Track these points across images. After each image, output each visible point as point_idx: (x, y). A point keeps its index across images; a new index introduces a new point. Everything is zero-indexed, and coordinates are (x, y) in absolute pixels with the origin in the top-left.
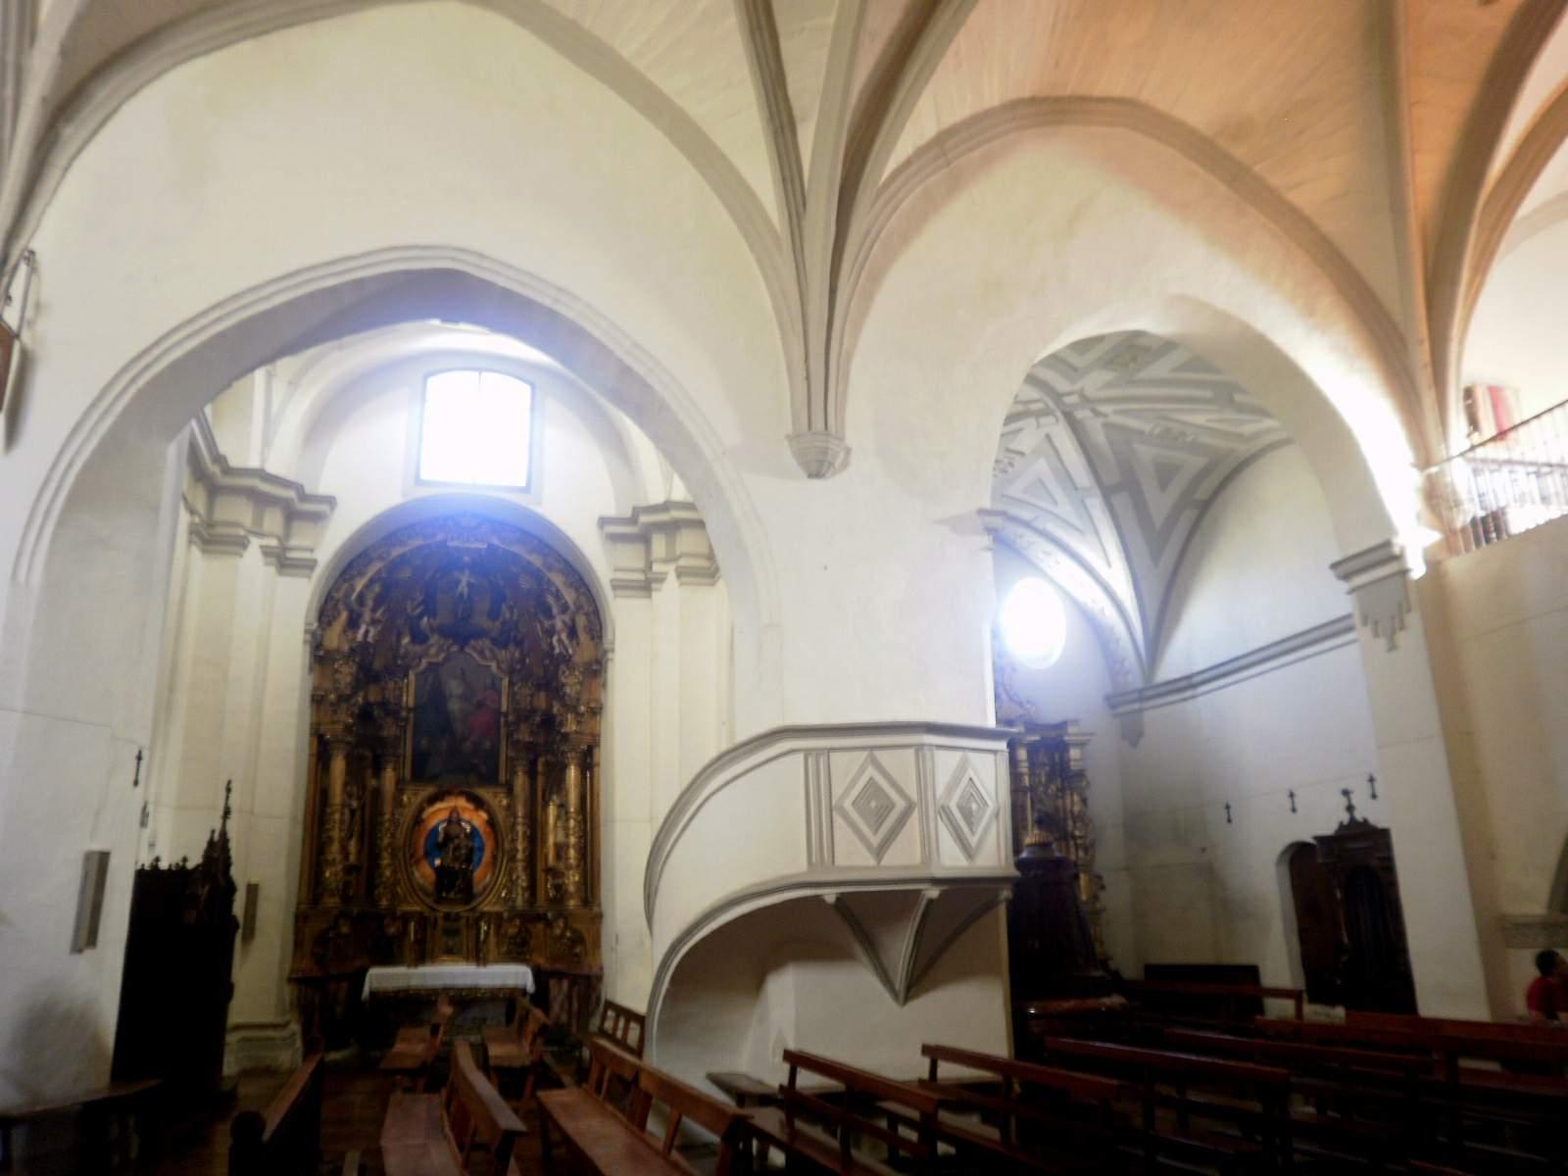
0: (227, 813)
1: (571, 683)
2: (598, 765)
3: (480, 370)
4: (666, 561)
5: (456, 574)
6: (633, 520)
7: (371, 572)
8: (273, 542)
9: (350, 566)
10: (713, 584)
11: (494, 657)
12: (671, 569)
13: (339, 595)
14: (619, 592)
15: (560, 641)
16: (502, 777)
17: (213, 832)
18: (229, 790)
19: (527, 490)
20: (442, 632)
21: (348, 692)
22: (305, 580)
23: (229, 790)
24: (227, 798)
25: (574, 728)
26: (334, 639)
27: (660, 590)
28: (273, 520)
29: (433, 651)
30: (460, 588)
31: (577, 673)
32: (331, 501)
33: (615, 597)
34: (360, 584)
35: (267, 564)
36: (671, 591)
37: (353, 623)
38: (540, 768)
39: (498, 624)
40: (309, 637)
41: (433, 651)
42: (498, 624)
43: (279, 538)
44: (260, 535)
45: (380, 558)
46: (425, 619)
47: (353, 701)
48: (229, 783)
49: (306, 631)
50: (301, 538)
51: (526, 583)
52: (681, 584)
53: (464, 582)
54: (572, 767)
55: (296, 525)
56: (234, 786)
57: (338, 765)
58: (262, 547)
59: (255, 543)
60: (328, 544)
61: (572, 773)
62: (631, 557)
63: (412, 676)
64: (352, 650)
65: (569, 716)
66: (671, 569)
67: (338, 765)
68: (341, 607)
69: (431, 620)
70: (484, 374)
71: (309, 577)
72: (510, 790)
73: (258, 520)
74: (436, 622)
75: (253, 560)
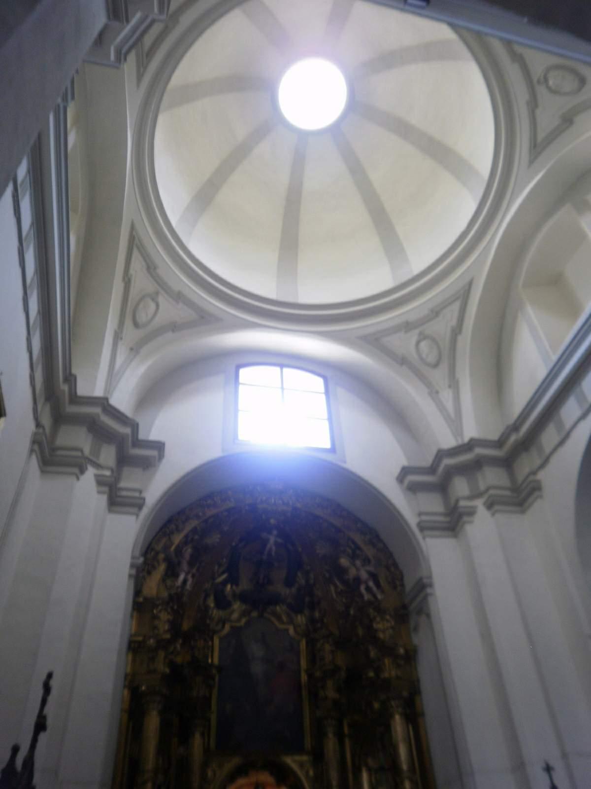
0: (41, 725)
1: (383, 627)
2: (423, 714)
3: (282, 366)
4: (471, 498)
5: (264, 535)
6: (432, 470)
7: (188, 527)
8: (107, 473)
9: (170, 521)
10: (523, 512)
11: (291, 621)
12: (479, 503)
13: (159, 547)
14: (427, 533)
15: (368, 589)
16: (308, 743)
17: (15, 749)
18: (47, 689)
19: (333, 450)
20: (243, 597)
21: (168, 636)
22: (134, 518)
23: (47, 689)
24: (44, 702)
25: (393, 673)
26: (152, 587)
27: (471, 522)
28: (108, 455)
29: (235, 616)
30: (268, 546)
31: (388, 617)
32: (159, 447)
33: (424, 538)
34: (177, 539)
35: (99, 492)
36: (483, 526)
37: (172, 572)
38: (346, 730)
39: (294, 590)
40: (134, 572)
41: (235, 616)
42: (294, 590)
43: (112, 471)
44: (98, 466)
45: (198, 517)
46: (229, 587)
47: (171, 649)
48: (50, 676)
49: (132, 566)
50: (130, 481)
51: (322, 549)
52: (493, 515)
53: (272, 539)
54: (397, 717)
55: (126, 470)
56: (53, 683)
57: (153, 722)
58: (96, 476)
59: (91, 472)
60: (156, 486)
61: (398, 725)
62: (433, 504)
63: (216, 641)
64: (171, 597)
65: (386, 661)
66: (479, 503)
67: (153, 722)
68: (161, 556)
69: (234, 587)
70: (285, 370)
71: (137, 516)
72: (318, 756)
73: (96, 452)
74: (238, 590)
75: (86, 490)
